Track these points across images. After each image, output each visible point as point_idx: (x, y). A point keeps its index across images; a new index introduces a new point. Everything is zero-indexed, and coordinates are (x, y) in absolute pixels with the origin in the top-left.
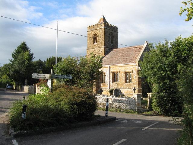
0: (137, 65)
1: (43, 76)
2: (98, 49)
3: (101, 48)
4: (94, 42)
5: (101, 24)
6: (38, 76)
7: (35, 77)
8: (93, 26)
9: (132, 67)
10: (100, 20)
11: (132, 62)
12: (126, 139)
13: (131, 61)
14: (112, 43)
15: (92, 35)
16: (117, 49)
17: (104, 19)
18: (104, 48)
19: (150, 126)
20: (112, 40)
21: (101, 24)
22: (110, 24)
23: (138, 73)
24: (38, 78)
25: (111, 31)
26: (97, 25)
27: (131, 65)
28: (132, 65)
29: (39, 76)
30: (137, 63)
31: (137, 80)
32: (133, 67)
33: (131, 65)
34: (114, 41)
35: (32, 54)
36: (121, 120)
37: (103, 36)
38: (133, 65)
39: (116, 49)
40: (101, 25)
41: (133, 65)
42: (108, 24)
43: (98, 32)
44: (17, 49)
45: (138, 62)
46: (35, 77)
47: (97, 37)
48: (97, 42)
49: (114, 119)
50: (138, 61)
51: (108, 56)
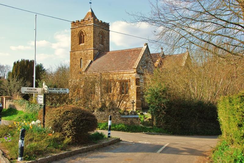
0: (135, 72)
1: (34, 91)
2: (85, 51)
3: (89, 51)
4: (80, 43)
5: (89, 19)
6: (28, 91)
7: (25, 92)
8: (79, 21)
9: (129, 75)
10: (88, 14)
11: (129, 68)
12: (89, 134)
13: (128, 67)
14: (103, 44)
15: (76, 34)
16: (109, 52)
17: (92, 13)
18: (92, 50)
19: (163, 148)
20: (103, 41)
21: (89, 19)
22: (99, 20)
23: (136, 82)
24: (28, 92)
25: (101, 30)
26: (84, 20)
27: (128, 72)
28: (129, 72)
29: (30, 91)
30: (135, 71)
31: (136, 91)
32: (131, 74)
33: (128, 72)
34: (105, 42)
35: (45, 69)
36: (131, 142)
37: (92, 35)
38: (131, 72)
39: (108, 53)
40: (89, 21)
41: (131, 72)
42: (98, 20)
43: (85, 29)
44: (20, 60)
45: (137, 68)
46: (25, 92)
47: (84, 36)
48: (83, 43)
49: (118, 140)
50: (136, 68)
51: (98, 60)
